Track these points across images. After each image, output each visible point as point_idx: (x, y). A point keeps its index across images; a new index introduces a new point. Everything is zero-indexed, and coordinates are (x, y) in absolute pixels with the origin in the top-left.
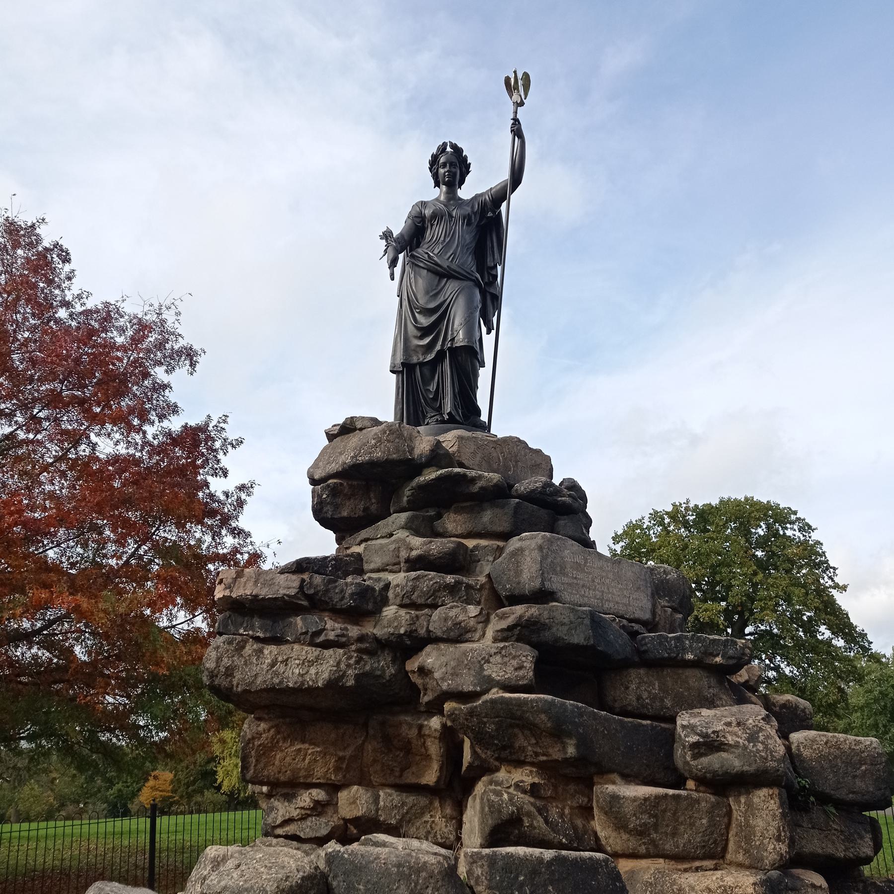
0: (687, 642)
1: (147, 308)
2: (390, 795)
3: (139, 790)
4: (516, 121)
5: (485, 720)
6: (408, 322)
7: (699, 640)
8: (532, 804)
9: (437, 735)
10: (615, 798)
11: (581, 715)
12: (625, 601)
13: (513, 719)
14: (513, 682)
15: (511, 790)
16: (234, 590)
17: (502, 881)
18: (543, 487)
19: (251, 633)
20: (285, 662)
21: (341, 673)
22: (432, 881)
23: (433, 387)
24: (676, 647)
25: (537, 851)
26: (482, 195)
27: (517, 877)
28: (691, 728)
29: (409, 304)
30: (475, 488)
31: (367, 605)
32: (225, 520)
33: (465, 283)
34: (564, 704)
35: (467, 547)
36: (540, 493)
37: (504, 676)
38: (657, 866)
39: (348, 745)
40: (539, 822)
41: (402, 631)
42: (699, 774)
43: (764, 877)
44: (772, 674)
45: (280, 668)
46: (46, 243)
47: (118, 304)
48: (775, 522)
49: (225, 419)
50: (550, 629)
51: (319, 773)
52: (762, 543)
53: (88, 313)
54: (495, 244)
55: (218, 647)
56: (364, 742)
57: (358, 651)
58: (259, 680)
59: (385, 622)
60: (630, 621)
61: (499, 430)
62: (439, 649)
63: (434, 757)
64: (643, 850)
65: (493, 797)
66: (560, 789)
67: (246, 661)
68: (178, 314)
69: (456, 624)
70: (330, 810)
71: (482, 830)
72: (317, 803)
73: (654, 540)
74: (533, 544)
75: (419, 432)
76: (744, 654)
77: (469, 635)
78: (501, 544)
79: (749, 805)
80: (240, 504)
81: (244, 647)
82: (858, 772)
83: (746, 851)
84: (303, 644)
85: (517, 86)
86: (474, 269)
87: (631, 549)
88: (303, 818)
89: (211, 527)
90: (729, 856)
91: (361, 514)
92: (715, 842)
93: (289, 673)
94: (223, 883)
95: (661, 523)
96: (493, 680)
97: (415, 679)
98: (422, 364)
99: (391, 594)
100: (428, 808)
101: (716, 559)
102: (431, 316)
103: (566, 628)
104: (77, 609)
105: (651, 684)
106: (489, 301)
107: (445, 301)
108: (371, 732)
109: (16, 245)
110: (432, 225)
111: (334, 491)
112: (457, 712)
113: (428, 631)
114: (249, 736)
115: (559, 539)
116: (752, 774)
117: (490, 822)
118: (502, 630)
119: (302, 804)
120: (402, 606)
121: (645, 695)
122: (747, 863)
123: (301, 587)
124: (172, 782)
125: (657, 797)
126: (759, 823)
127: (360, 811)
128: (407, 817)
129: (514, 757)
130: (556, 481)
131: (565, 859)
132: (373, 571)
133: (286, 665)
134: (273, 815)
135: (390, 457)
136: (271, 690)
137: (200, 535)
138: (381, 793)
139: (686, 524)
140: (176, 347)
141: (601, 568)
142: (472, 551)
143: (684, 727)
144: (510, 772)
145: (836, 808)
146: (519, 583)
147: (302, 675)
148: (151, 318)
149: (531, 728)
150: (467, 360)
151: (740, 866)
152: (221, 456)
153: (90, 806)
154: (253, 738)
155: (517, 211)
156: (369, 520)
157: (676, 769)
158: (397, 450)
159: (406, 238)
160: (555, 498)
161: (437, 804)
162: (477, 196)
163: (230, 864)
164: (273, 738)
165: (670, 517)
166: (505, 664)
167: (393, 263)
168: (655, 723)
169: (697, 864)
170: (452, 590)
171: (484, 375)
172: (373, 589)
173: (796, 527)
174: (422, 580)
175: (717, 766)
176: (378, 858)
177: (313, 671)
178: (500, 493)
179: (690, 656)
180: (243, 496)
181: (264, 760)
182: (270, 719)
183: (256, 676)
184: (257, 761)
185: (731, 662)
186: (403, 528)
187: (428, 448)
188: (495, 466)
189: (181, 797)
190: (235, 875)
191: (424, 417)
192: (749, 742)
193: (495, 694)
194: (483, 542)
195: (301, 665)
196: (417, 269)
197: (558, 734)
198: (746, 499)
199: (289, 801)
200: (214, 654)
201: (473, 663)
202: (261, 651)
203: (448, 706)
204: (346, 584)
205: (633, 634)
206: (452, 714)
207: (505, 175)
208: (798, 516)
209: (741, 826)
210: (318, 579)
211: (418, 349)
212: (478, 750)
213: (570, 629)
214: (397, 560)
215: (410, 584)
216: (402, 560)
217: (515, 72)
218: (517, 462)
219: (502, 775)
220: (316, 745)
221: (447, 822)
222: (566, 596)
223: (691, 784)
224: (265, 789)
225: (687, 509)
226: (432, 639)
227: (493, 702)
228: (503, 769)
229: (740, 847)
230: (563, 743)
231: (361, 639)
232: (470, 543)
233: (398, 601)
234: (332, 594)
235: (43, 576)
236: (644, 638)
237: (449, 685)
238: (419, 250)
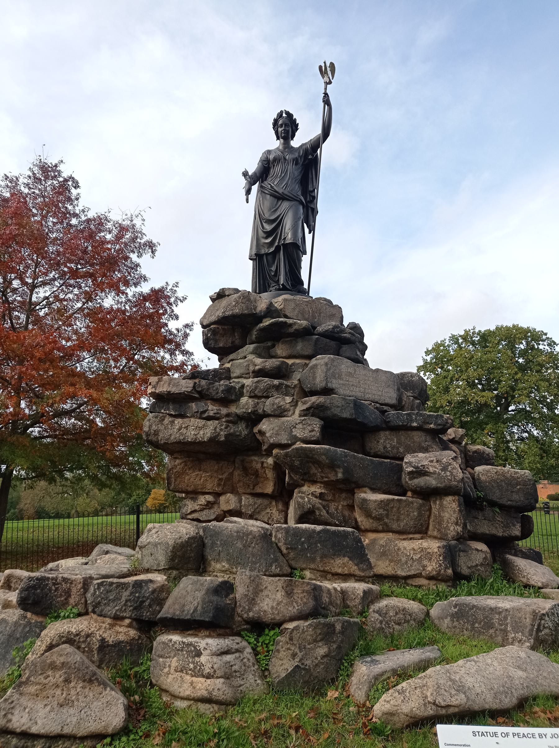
0: (414, 416)
1: (124, 217)
2: (248, 499)
3: (146, 499)
4: (326, 94)
5: (294, 459)
6: (259, 228)
7: (421, 415)
8: (320, 503)
9: (272, 467)
10: (365, 500)
11: (346, 456)
12: (380, 393)
13: (308, 458)
14: (308, 439)
15: (310, 496)
17: (292, 541)
18: (333, 328)
19: (167, 412)
20: (186, 428)
22: (255, 540)
23: (273, 268)
24: (407, 419)
25: (312, 526)
26: (306, 144)
27: (301, 539)
28: (410, 463)
29: (260, 217)
30: (291, 330)
31: (230, 397)
32: (178, 346)
33: (293, 203)
34: (336, 450)
35: (288, 364)
36: (331, 332)
38: (388, 537)
39: (225, 472)
40: (324, 512)
41: (250, 411)
42: (413, 488)
43: (445, 544)
44: (525, 435)
45: (184, 431)
46: (65, 175)
47: (106, 214)
48: (532, 340)
49: (176, 285)
50: (330, 409)
51: (210, 486)
52: (523, 354)
53: (88, 221)
54: (314, 176)
55: (150, 420)
56: (233, 471)
57: (226, 421)
58: (172, 437)
59: (241, 406)
60: (381, 404)
61: (314, 294)
62: (269, 421)
63: (270, 479)
64: (380, 528)
65: (300, 500)
66: (337, 496)
68: (144, 220)
69: (279, 407)
70: (216, 506)
71: (295, 517)
72: (209, 502)
73: (452, 353)
74: (322, 362)
75: (260, 297)
76: (447, 423)
78: (307, 362)
79: (441, 505)
80: (186, 336)
81: (164, 420)
82: (515, 489)
83: (439, 530)
85: (327, 71)
86: (300, 193)
87: (436, 359)
88: (202, 510)
89: (169, 350)
90: (429, 533)
91: (230, 345)
92: (421, 525)
93: (188, 434)
94: (148, 541)
95: (457, 342)
96: (297, 437)
97: (259, 437)
98: (267, 254)
99: (245, 391)
101: (490, 365)
102: (272, 224)
103: (339, 409)
104: (91, 398)
106: (309, 213)
108: (237, 465)
109: (47, 178)
110: (274, 166)
111: (214, 332)
113: (264, 411)
114: (170, 467)
115: (338, 359)
116: (442, 488)
117: (299, 512)
118: (304, 410)
119: (200, 503)
120: (250, 397)
121: (388, 446)
122: (439, 536)
123: (194, 387)
124: (164, 495)
125: (388, 500)
126: (446, 515)
129: (311, 479)
130: (346, 323)
131: (328, 531)
132: (235, 378)
133: (187, 429)
134: (186, 508)
136: (179, 443)
137: (163, 355)
138: (243, 498)
139: (473, 343)
140: (142, 241)
141: (365, 375)
142: (291, 366)
143: (406, 463)
144: (309, 487)
145: (500, 509)
146: (314, 384)
147: (196, 435)
148: (127, 223)
149: (318, 463)
150: (294, 252)
151: (435, 538)
152: (174, 308)
153: (119, 509)
154: (172, 468)
155: (328, 153)
156: (235, 348)
157: (402, 486)
158: (247, 308)
159: (258, 175)
160: (340, 334)
161: (274, 503)
162: (303, 145)
163: (154, 531)
165: (463, 339)
166: (304, 429)
167: (248, 192)
168: (392, 461)
169: (411, 536)
170: (278, 388)
171: (305, 260)
172: (235, 388)
173: (545, 343)
174: (260, 383)
176: (227, 528)
177: (201, 432)
178: (306, 333)
179: (415, 424)
180: (188, 331)
181: (179, 480)
182: (181, 458)
183: (171, 435)
185: (439, 427)
186: (251, 353)
188: (307, 316)
189: (170, 504)
190: (154, 537)
191: (269, 286)
192: (442, 471)
193: (298, 445)
194: (297, 361)
195: (195, 429)
196: (264, 194)
197: (333, 466)
198: (514, 326)
199: (194, 502)
200: (147, 423)
201: (287, 428)
202: (173, 422)
203: (275, 451)
204: (220, 385)
205: (383, 412)
206: (277, 456)
207: (318, 131)
208: (547, 336)
210: (203, 382)
211: (265, 245)
212: (293, 476)
213: (342, 409)
215: (254, 385)
216: (251, 371)
217: (325, 63)
218: (320, 313)
219: (305, 488)
220: (207, 472)
221: (279, 513)
222: (341, 391)
223: (409, 494)
224: (184, 495)
225: (474, 333)
226: (266, 415)
227: (297, 449)
228: (306, 485)
229: (435, 527)
230: (335, 471)
231: (228, 415)
232: (290, 362)
233: (248, 395)
234: (211, 391)
235: (71, 379)
236: (389, 414)
238: (266, 182)
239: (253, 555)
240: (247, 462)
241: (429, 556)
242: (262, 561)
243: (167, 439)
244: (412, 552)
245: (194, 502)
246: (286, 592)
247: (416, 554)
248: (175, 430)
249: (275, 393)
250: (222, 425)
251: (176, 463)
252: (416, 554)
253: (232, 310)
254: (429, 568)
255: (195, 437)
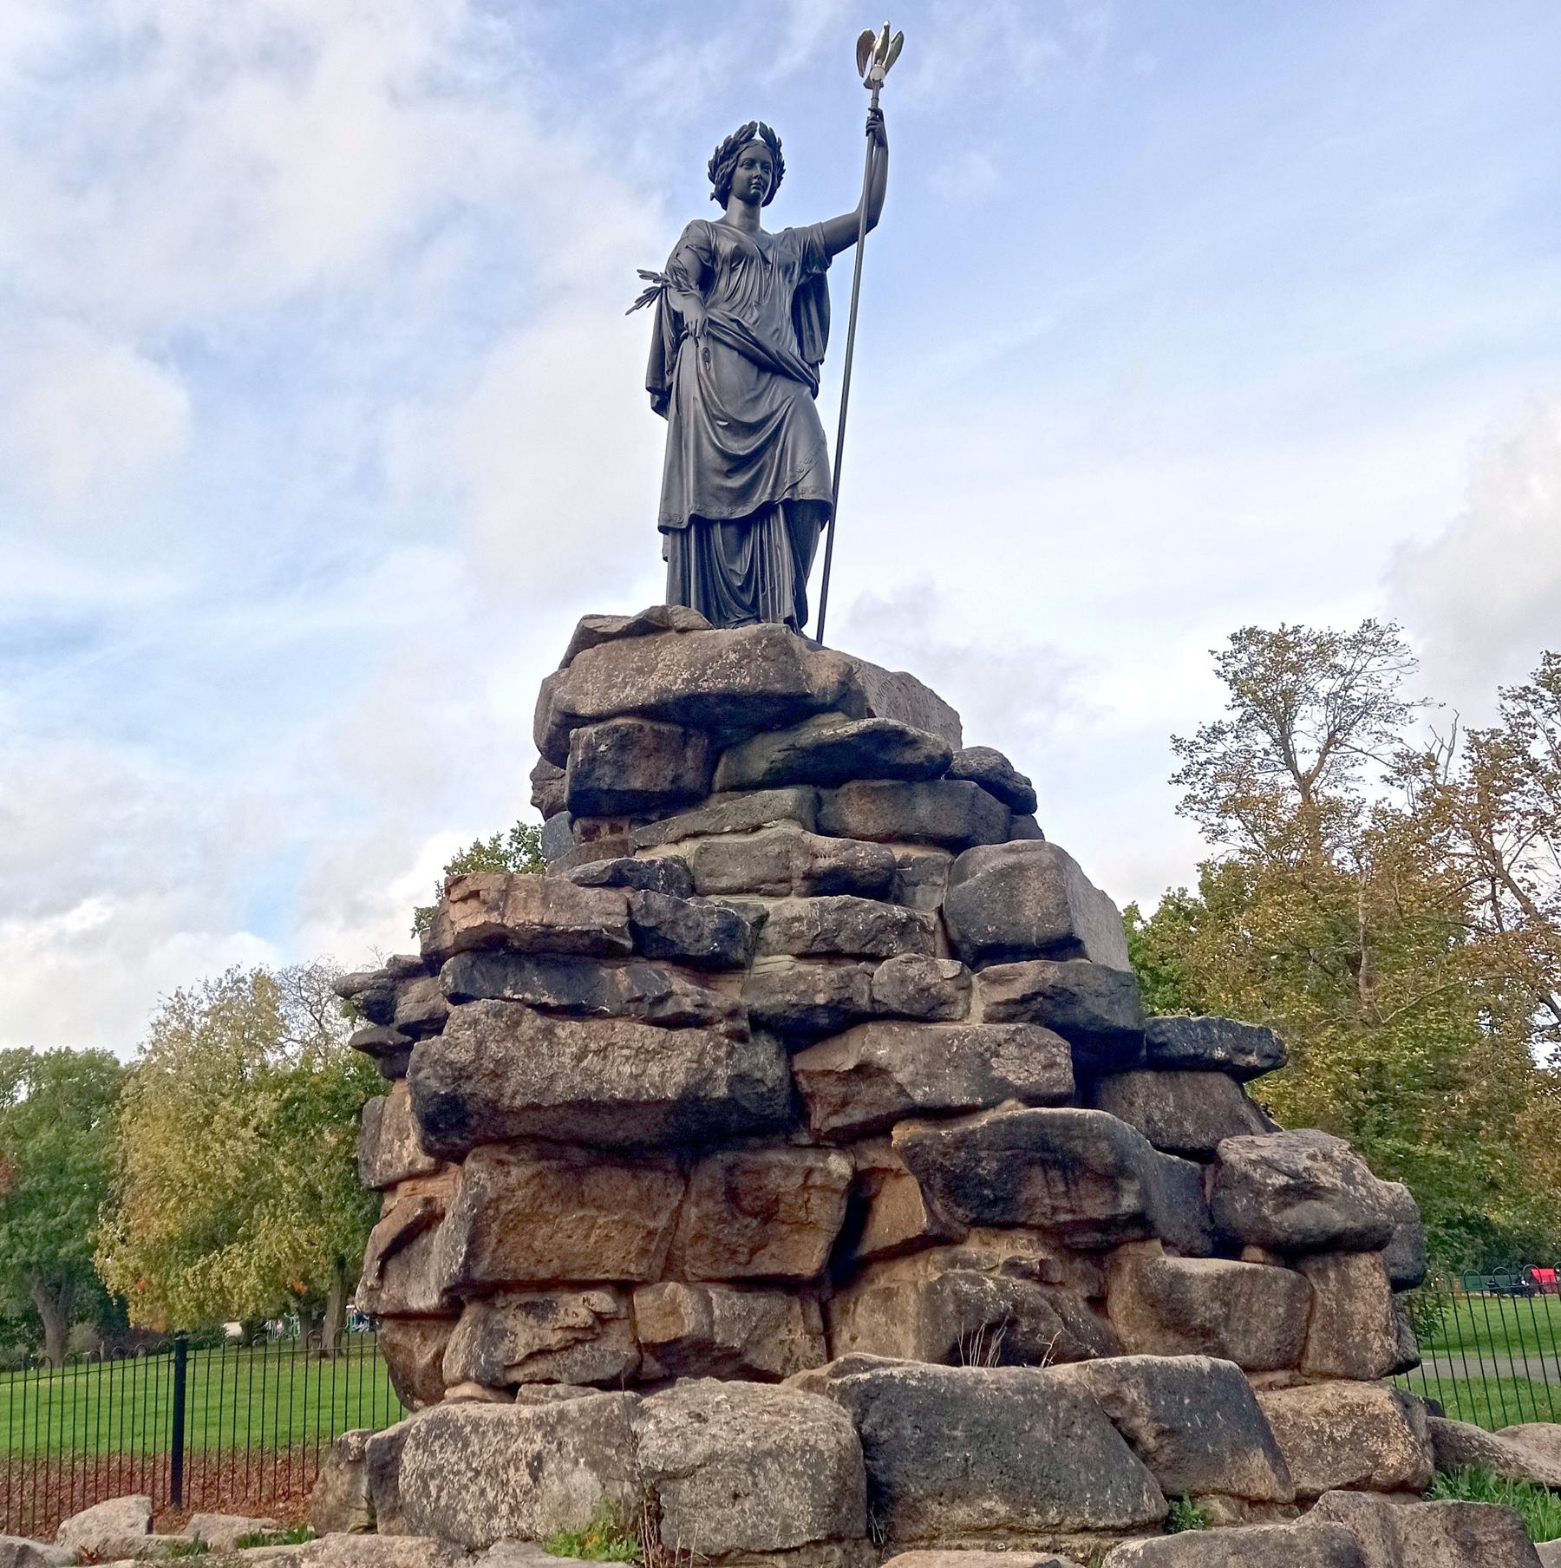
6: (705, 441)
8: (1043, 1296)
9: (842, 1185)
16: (508, 913)
21: (705, 1074)
23: (741, 567)
30: (910, 757)
37: (1027, 1078)
39: (660, 1209)
41: (820, 999)
57: (730, 1035)
58: (560, 1086)
62: (891, 1033)
65: (966, 1287)
67: (527, 1050)
69: (923, 990)
77: (945, 1010)
79: (1344, 1280)
81: (518, 1023)
83: (1339, 1353)
84: (633, 1020)
90: (1308, 1364)
91: (666, 786)
96: (1010, 1085)
98: (725, 523)
100: (781, 1320)
105: (1163, 1098)
107: (774, 413)
112: (927, 1142)
113: (873, 1001)
118: (1007, 1003)
119: (570, 1321)
121: (1157, 1116)
122: (1339, 1371)
126: (1359, 1308)
127: (689, 1323)
128: (755, 1337)
133: (605, 1057)
134: (506, 1344)
135: (769, 687)
154: (499, 1198)
161: (797, 1308)
164: (534, 1197)
166: (1025, 1059)
174: (851, 911)
175: (1310, 1223)
177: (654, 1069)
179: (1219, 1054)
181: (511, 1239)
184: (500, 1241)
186: (788, 817)
187: (835, 678)
193: (1011, 1109)
194: (915, 853)
203: (900, 1134)
209: (1331, 1316)
210: (659, 901)
211: (721, 494)
214: (785, 874)
217: (887, 28)
219: (972, 1249)
221: (814, 1339)
229: (1329, 1347)
234: (682, 930)
237: (925, 1093)
239: (1088, 1465)
240: (745, 1173)
241: (1376, 1425)
242: (1116, 1480)
243: (540, 1093)
244: (1324, 1420)
245: (544, 1318)
246: (1462, 1544)
247: (1338, 1423)
248: (566, 1060)
249: (896, 947)
250: (718, 1046)
251: (512, 1180)
252: (1338, 1423)
253: (728, 677)
254: (1392, 1460)
255: (634, 1084)
